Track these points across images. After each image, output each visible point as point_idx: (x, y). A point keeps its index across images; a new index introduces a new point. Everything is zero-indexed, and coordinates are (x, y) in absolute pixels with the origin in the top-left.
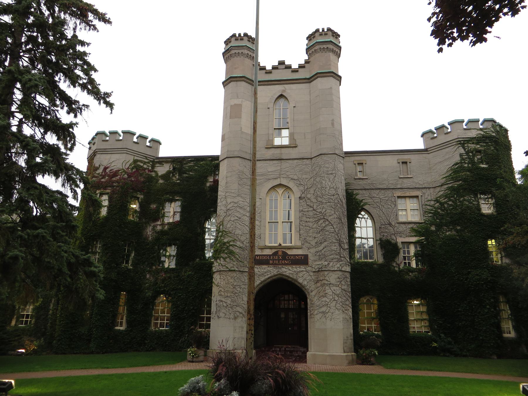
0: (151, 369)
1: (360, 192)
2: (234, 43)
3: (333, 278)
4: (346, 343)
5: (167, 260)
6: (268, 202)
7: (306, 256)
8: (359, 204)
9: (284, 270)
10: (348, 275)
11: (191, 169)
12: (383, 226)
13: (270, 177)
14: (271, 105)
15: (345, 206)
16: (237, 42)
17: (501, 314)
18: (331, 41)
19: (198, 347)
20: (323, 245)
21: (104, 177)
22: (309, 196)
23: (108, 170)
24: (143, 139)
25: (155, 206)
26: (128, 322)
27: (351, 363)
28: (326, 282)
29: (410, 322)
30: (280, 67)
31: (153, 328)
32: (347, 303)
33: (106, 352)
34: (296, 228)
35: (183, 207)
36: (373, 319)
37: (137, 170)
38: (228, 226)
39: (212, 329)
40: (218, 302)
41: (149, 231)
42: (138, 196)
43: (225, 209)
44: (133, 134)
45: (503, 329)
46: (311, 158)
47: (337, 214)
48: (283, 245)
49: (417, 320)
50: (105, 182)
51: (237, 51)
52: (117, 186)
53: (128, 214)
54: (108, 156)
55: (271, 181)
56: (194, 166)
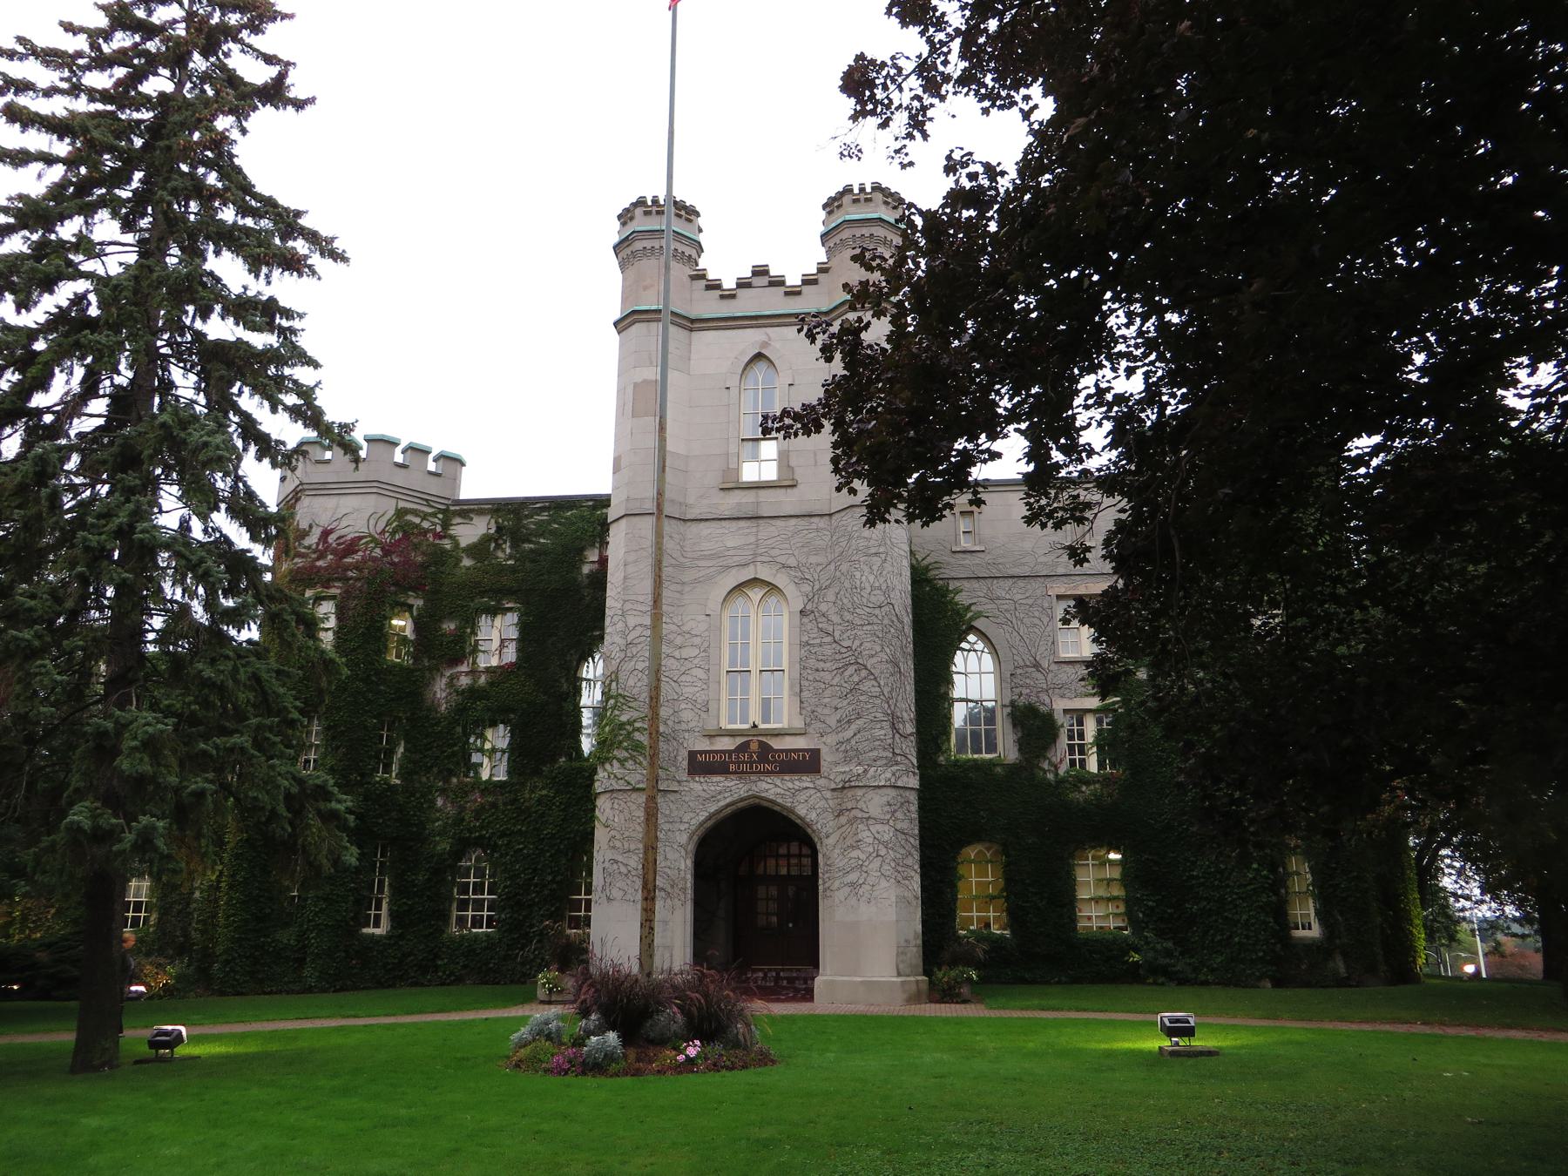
0: (455, 1017)
1: (966, 584)
2: (640, 223)
3: (875, 804)
4: (903, 953)
5: (486, 760)
6: (726, 623)
7: (815, 754)
8: (962, 616)
9: (764, 785)
10: (913, 797)
11: (542, 530)
12: (1019, 671)
13: (730, 562)
14: (733, 381)
15: (909, 631)
16: (648, 218)
17: (1289, 883)
18: (880, 219)
19: (562, 970)
20: (854, 727)
21: (322, 556)
22: (823, 607)
23: (331, 538)
24: (420, 455)
25: (452, 626)
26: (393, 916)
27: (915, 999)
28: (860, 815)
29: (1079, 905)
30: (758, 281)
31: (454, 929)
32: (909, 861)
33: (342, 989)
34: (791, 687)
35: (523, 627)
36: (993, 898)
37: (406, 535)
38: (631, 682)
39: (595, 932)
40: (607, 865)
41: (440, 690)
42: (410, 601)
43: (622, 642)
44: (394, 444)
45: (1291, 919)
46: (830, 515)
47: (889, 651)
48: (762, 726)
49: (1097, 900)
50: (326, 569)
51: (648, 244)
52: (357, 579)
53: (386, 647)
54: (331, 502)
55: (734, 571)
56: (549, 523)
